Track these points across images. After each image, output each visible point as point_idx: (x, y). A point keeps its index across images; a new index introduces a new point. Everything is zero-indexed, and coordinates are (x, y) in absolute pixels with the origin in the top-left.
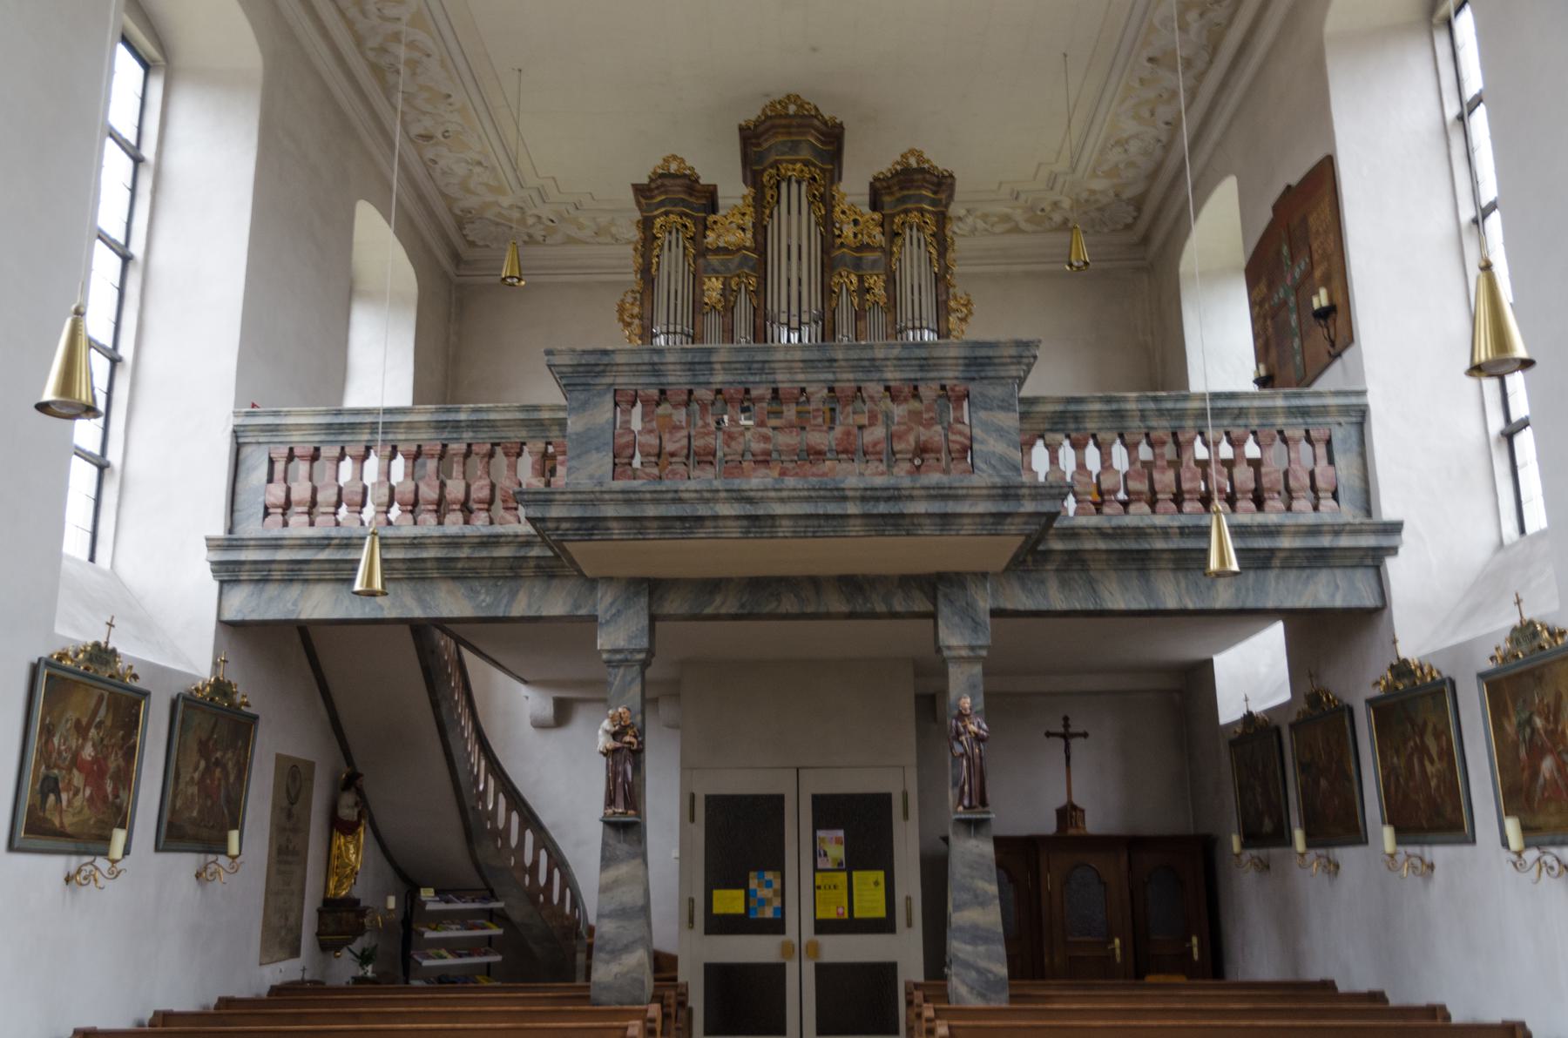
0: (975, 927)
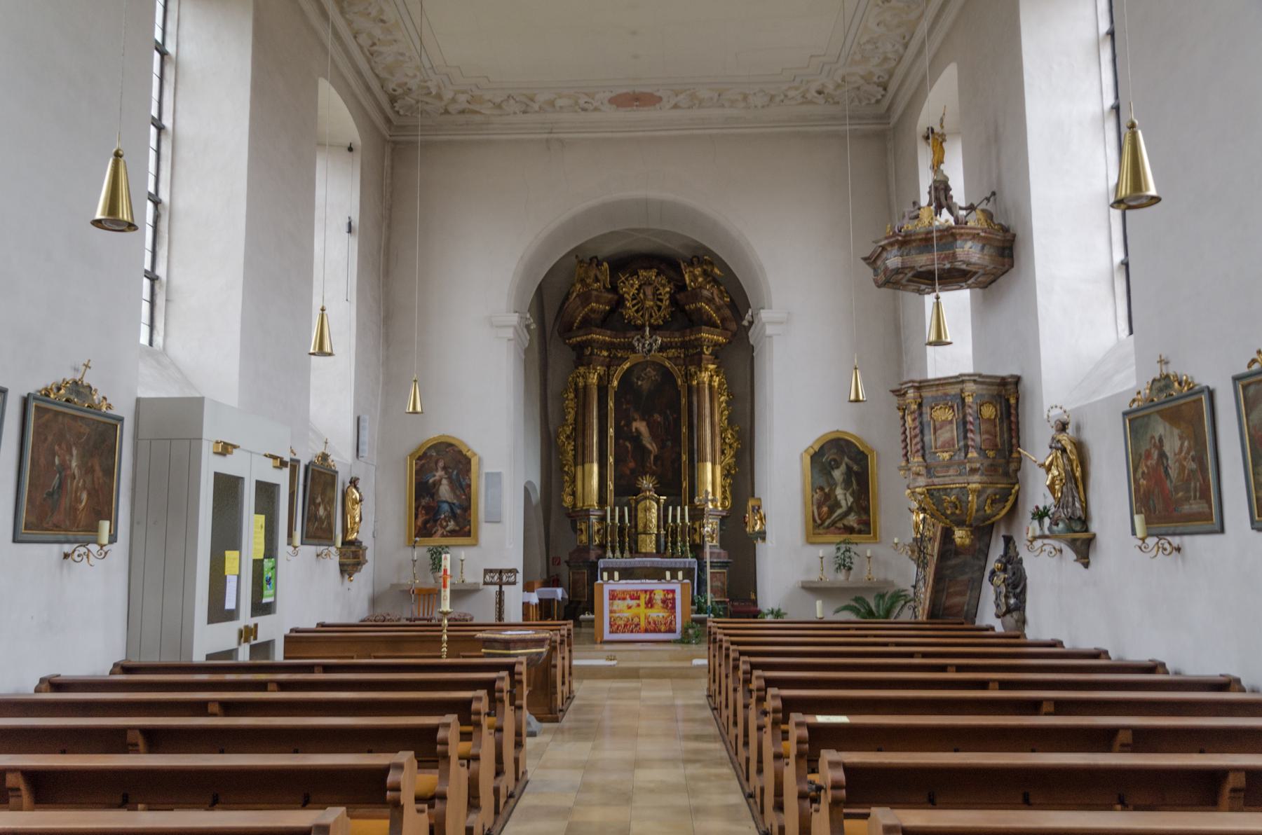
0: (829, 524)
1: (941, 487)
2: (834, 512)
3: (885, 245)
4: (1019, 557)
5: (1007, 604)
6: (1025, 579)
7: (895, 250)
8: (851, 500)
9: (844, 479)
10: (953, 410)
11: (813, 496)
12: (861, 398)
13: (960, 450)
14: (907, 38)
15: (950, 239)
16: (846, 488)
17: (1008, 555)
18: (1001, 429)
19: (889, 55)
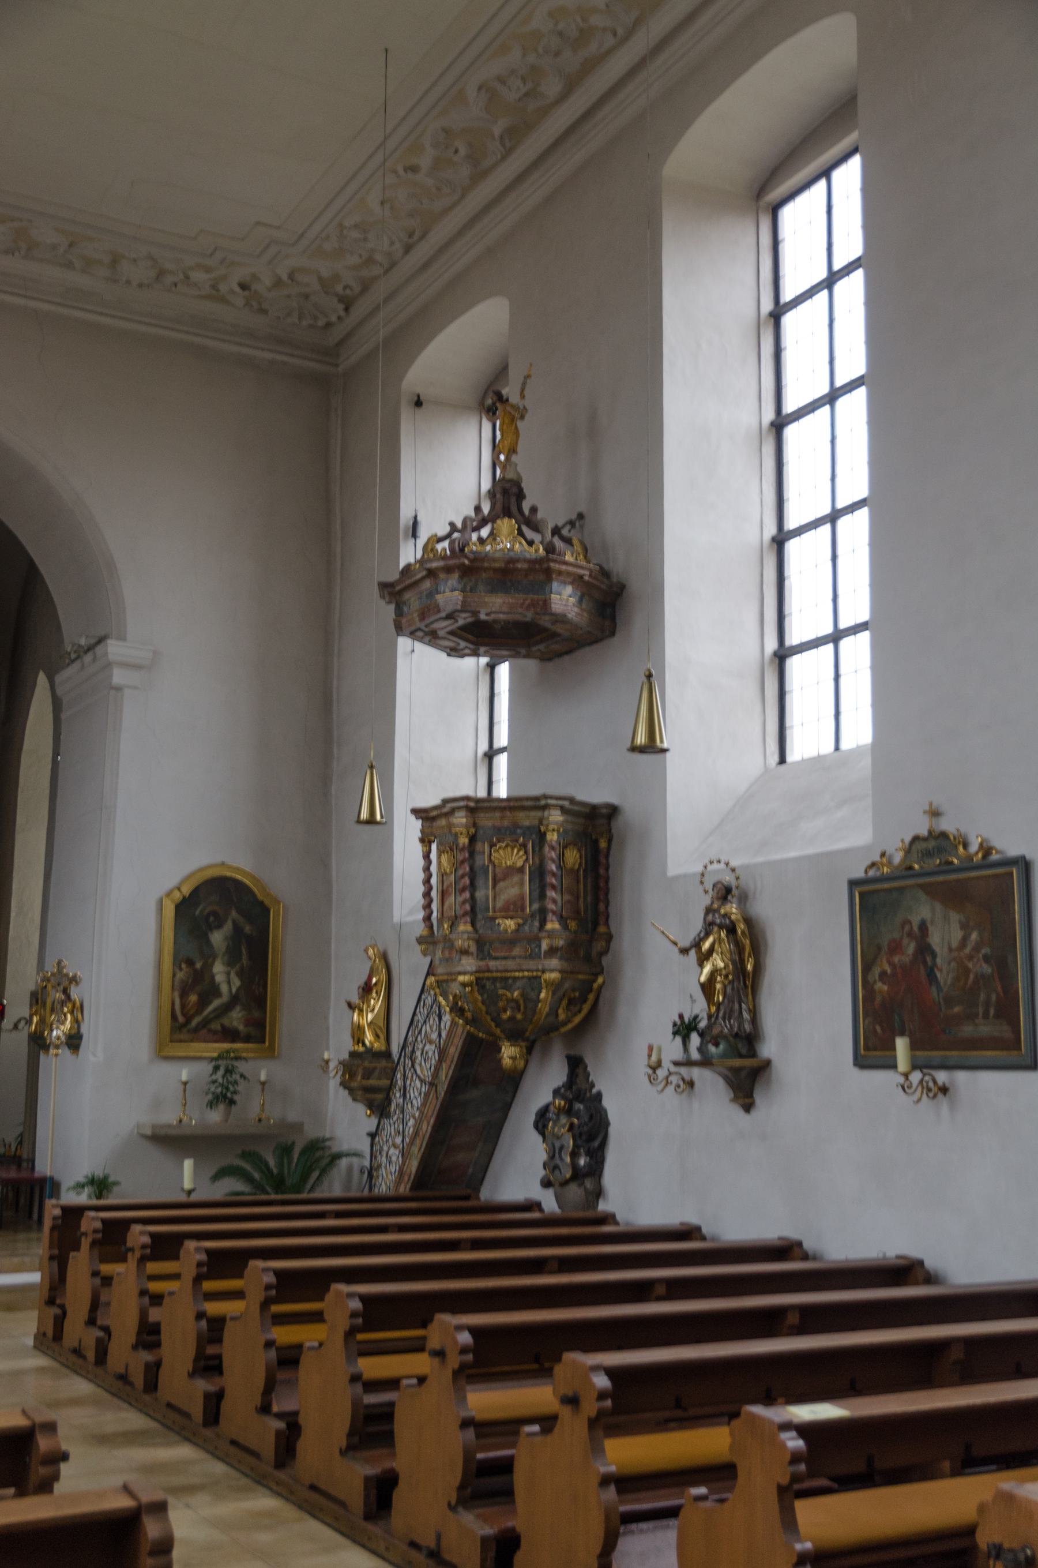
1: (499, 975)
2: (210, 1003)
3: (437, 569)
4: (594, 1091)
5: (574, 1166)
6: (607, 1124)
7: (453, 580)
8: (236, 983)
9: (228, 947)
10: (526, 852)
11: (174, 975)
12: (378, 818)
13: (532, 916)
14: (416, 237)
15: (542, 577)
16: (230, 964)
17: (574, 1088)
18: (585, 886)
19: (378, 257)
